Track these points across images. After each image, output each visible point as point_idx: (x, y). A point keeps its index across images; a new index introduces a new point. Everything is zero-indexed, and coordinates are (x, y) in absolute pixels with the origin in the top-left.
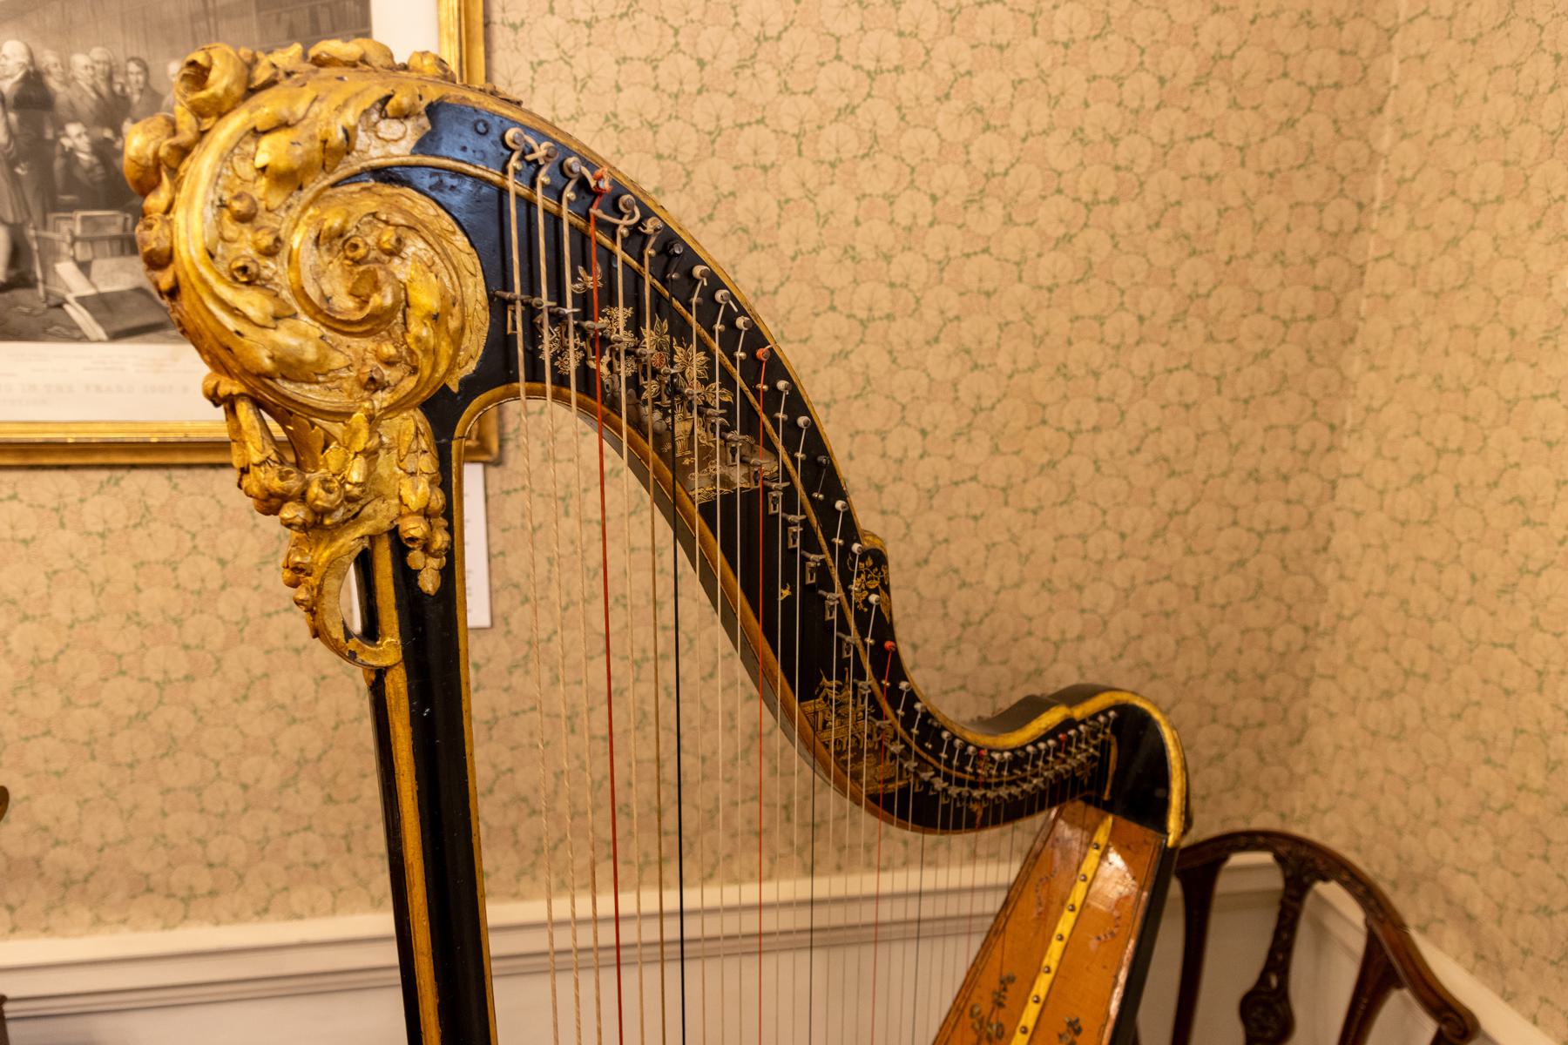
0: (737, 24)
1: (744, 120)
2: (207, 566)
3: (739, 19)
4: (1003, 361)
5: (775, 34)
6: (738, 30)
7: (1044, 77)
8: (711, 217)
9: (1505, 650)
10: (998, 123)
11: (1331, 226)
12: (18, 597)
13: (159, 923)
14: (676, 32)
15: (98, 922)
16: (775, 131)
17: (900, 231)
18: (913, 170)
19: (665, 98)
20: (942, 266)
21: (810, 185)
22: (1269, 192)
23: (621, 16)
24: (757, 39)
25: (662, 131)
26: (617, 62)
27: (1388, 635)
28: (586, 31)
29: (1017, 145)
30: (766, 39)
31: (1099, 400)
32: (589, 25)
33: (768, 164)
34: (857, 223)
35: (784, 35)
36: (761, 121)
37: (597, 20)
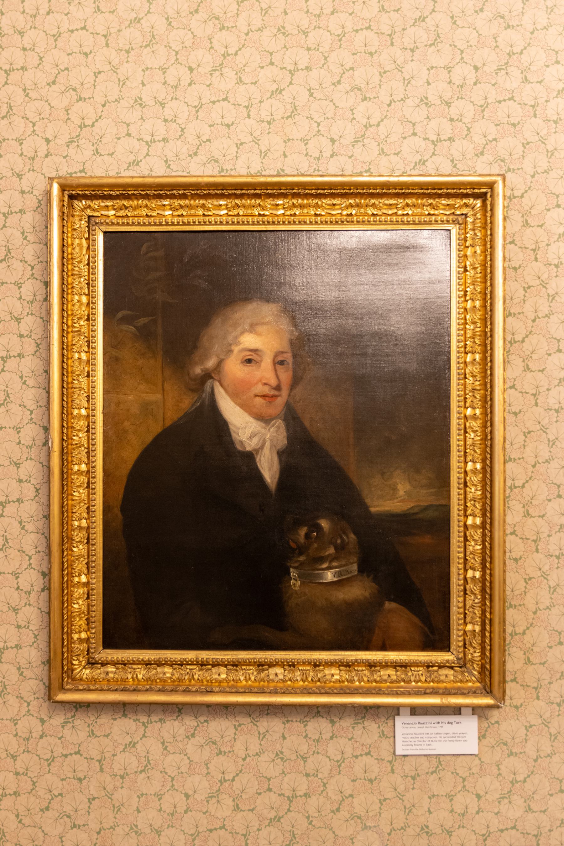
0: (212, 48)
1: (358, 754)
4: (530, 749)
8: (54, 82)
10: (87, 97)
11: (457, 80)
14: (319, 125)
16: (377, 759)
17: (170, 88)
20: (483, 108)
23: (288, 118)
25: (310, 35)
26: (285, 142)
29: (240, 762)
32: (269, 123)
37: (274, 120)
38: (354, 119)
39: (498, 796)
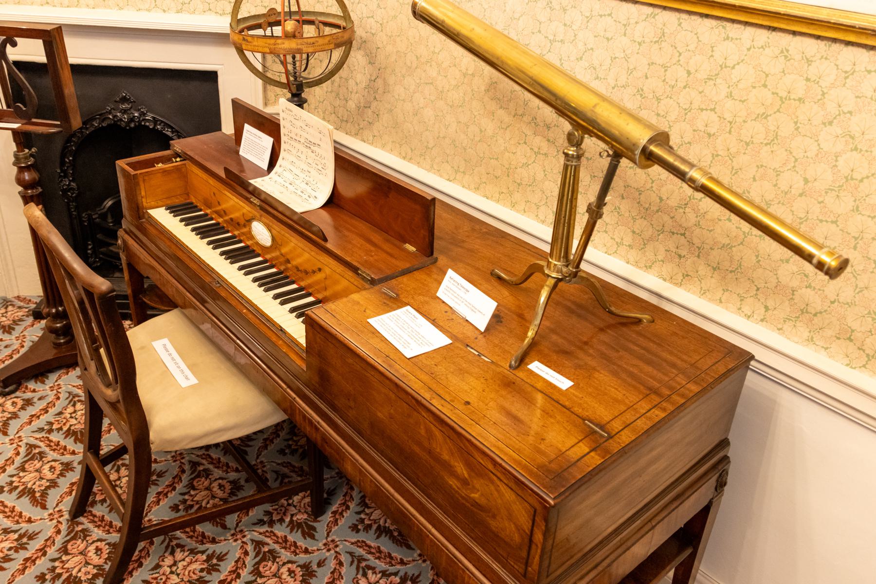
0: (712, 56)
2: (682, 74)
5: (732, 65)
6: (712, 59)
12: (857, 135)
13: (847, 361)
14: (680, 54)
15: (811, 340)
18: (796, 160)
19: (667, 87)
28: (638, 47)
30: (726, 67)
33: (712, 133)
34: (754, 179)
35: (737, 67)
36: (713, 110)
38: (712, 56)
39: (828, 187)
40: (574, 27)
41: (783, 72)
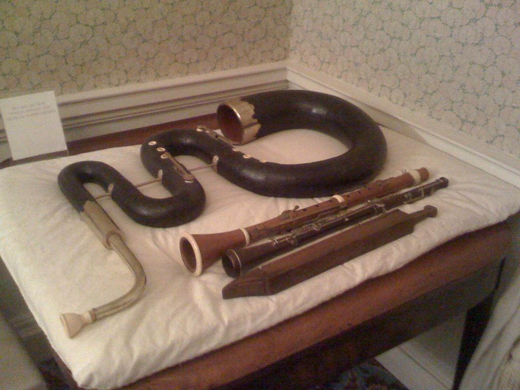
0: (30, 15)
3: (31, 12)
5: (49, 17)
7: (165, 18)
9: (356, 48)
21: (72, 75)
22: (253, 49)
24: (40, 20)
27: (315, 48)
31: (197, 49)
38: (30, 15)
40: (410, 27)
41: (86, 9)
